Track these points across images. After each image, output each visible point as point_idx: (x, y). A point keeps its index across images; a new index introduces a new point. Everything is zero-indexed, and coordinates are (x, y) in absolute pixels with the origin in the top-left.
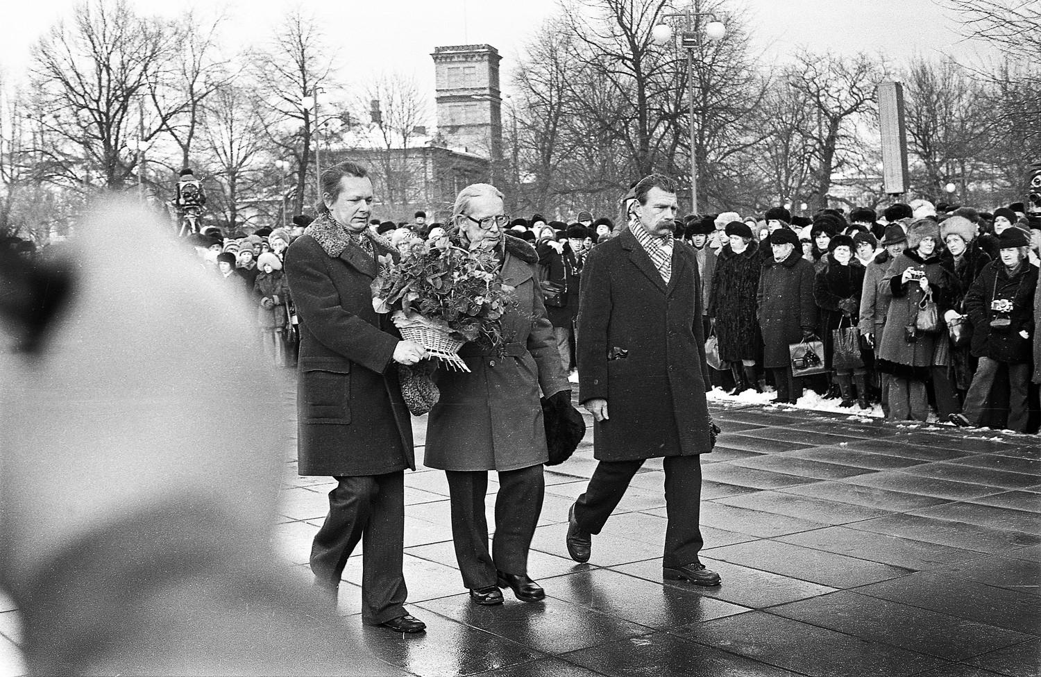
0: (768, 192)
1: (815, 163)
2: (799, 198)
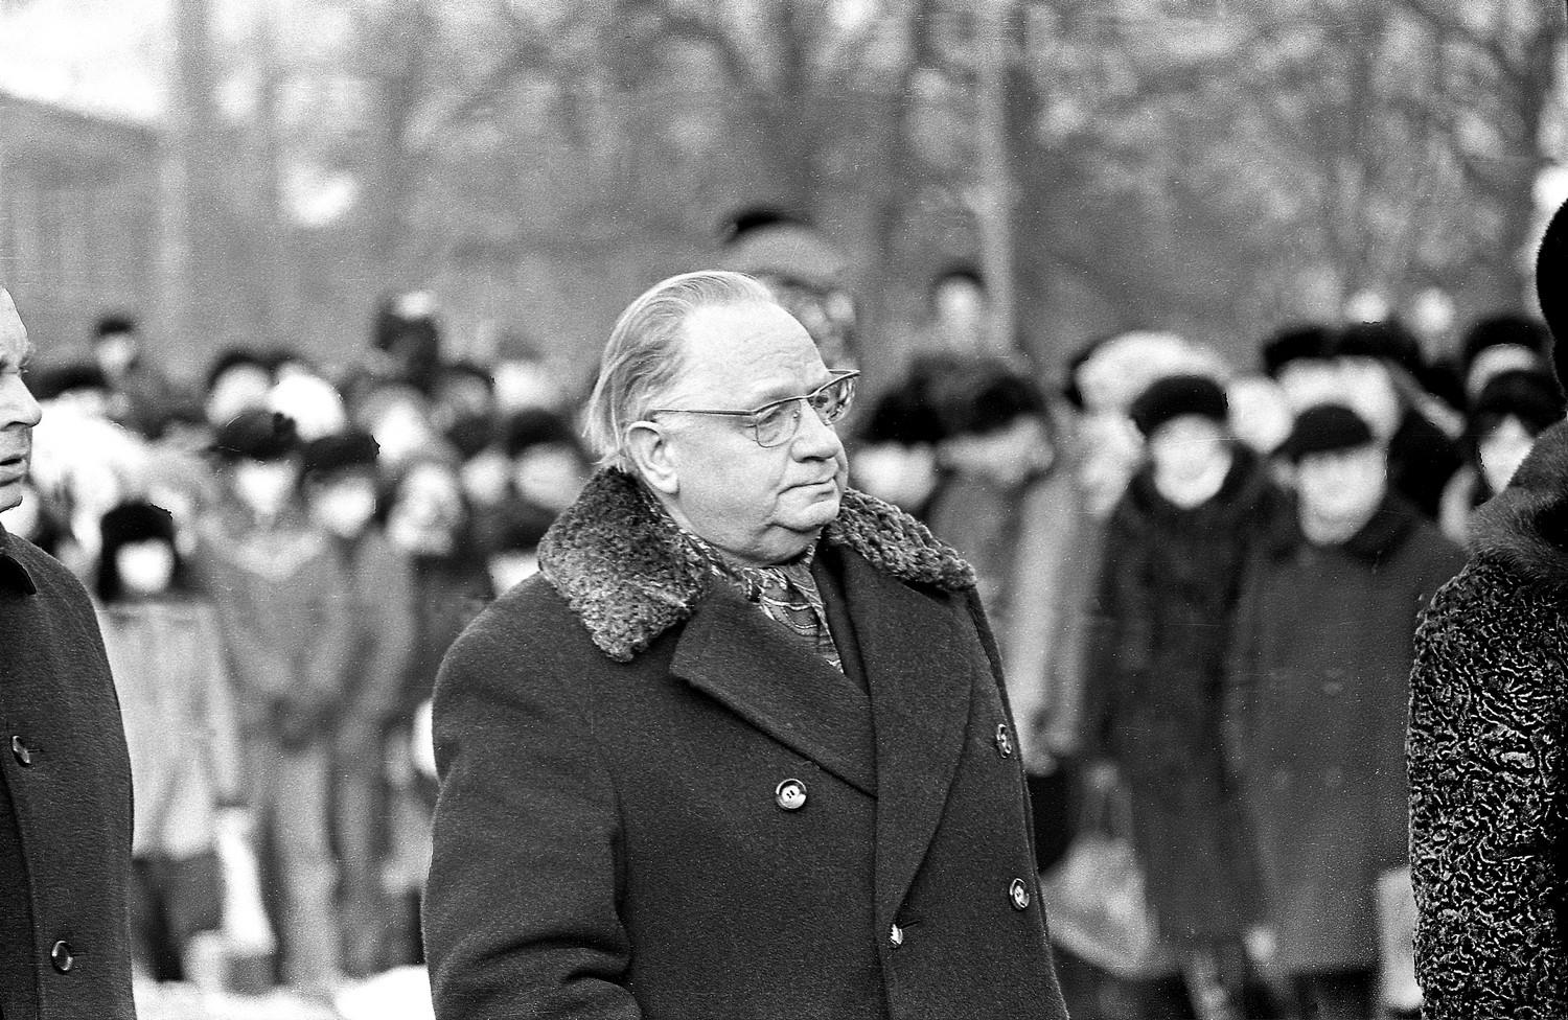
0: (1280, 251)
1: (1478, 134)
2: (1418, 277)
